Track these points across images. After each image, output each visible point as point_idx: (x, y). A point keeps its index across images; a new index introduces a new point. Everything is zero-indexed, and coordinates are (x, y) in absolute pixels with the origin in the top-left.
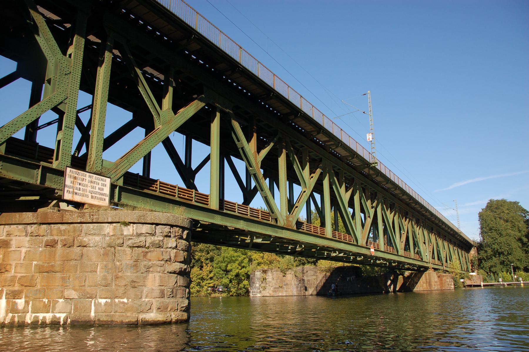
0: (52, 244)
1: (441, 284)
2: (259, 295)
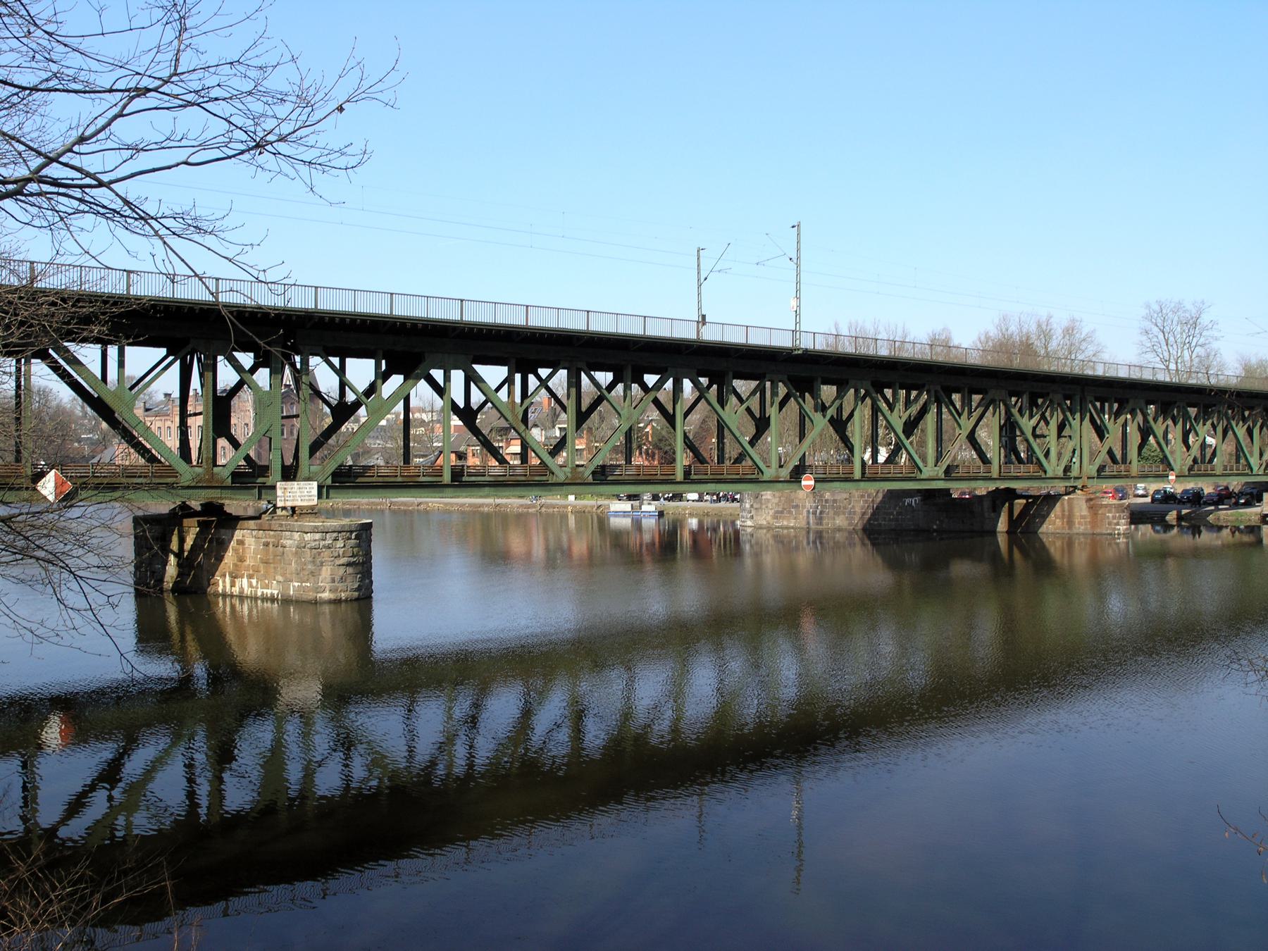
0: (266, 544)
1: (1094, 523)
2: (749, 523)
